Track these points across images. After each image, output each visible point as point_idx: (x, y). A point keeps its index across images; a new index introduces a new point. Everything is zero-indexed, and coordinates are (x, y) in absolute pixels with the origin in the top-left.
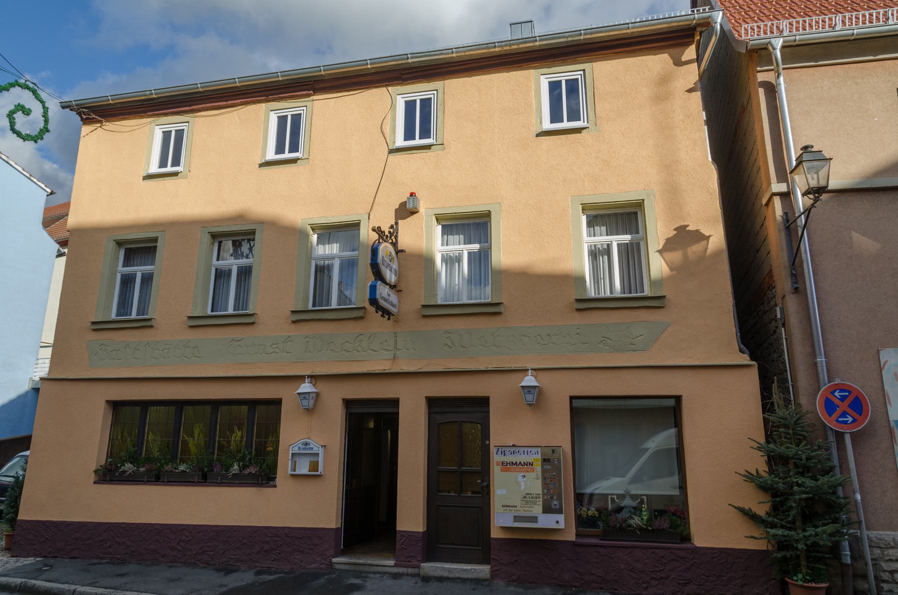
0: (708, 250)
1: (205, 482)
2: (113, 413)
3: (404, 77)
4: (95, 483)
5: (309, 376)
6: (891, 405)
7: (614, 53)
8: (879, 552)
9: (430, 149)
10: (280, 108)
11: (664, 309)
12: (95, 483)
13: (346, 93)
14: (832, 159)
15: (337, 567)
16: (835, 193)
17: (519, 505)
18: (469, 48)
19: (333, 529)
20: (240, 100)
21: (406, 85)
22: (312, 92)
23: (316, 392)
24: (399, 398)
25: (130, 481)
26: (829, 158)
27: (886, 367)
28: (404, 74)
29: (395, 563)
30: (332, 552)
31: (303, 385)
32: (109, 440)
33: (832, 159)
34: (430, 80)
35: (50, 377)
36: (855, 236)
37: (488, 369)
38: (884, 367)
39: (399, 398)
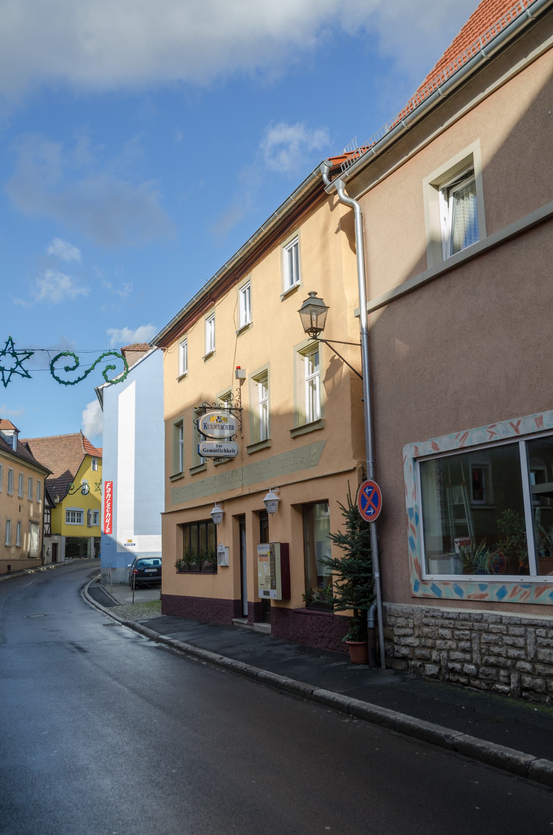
0: (343, 374)
1: (201, 572)
2: (183, 531)
3: (237, 276)
4: (177, 573)
5: (218, 503)
6: (407, 496)
7: (306, 214)
8: (394, 620)
9: (248, 328)
10: (209, 316)
11: (324, 430)
12: (177, 573)
13: (224, 297)
14: (329, 308)
15: (235, 624)
16: (388, 305)
17: (264, 584)
18: (228, 263)
19: (231, 600)
20: (195, 318)
21: (241, 280)
22: (213, 302)
23: (278, 500)
24: (245, 513)
25: (195, 572)
26: (327, 306)
27: (406, 460)
28: (236, 274)
29: (247, 623)
30: (232, 615)
31: (214, 509)
32: (184, 548)
33: (329, 308)
34: (247, 273)
35: (166, 512)
36: (397, 341)
37: (258, 491)
38: (405, 461)
39: (245, 513)
